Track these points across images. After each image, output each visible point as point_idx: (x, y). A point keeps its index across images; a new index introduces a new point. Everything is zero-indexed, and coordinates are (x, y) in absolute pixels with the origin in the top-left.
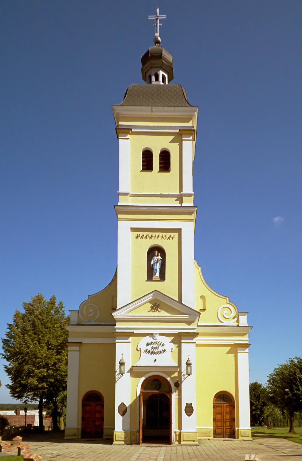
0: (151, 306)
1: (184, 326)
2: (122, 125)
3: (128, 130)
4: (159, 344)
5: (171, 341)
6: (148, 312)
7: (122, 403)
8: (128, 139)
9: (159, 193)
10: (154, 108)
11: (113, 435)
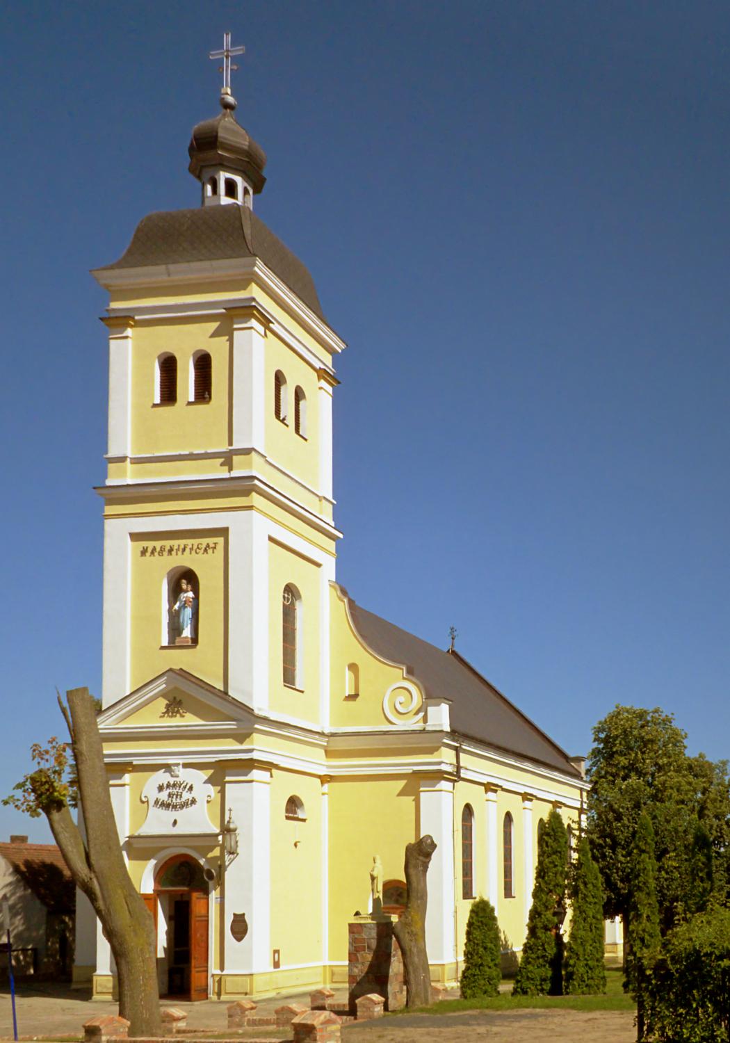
0: (167, 705)
1: (231, 744)
2: (114, 310)
3: (122, 321)
4: (182, 787)
5: (206, 778)
6: (161, 717)
8: (126, 337)
9: (187, 452)
11: (90, 981)
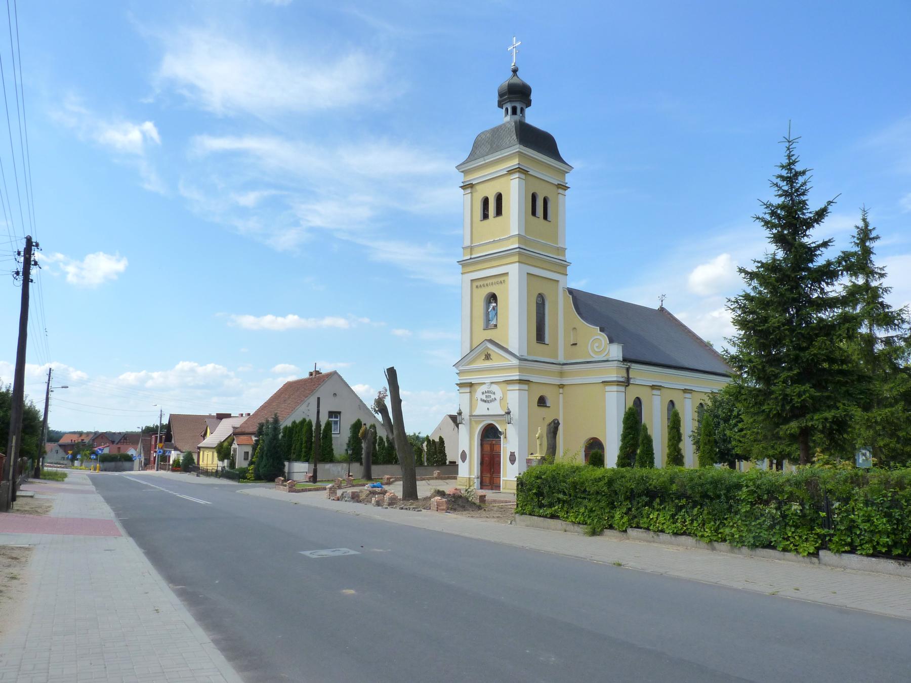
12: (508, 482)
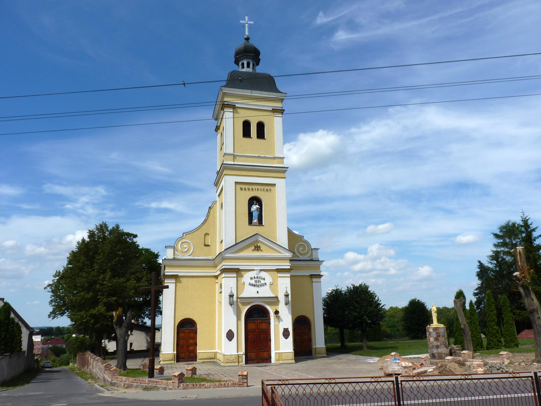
7: (230, 330)
10: (253, 91)
12: (226, 356)
